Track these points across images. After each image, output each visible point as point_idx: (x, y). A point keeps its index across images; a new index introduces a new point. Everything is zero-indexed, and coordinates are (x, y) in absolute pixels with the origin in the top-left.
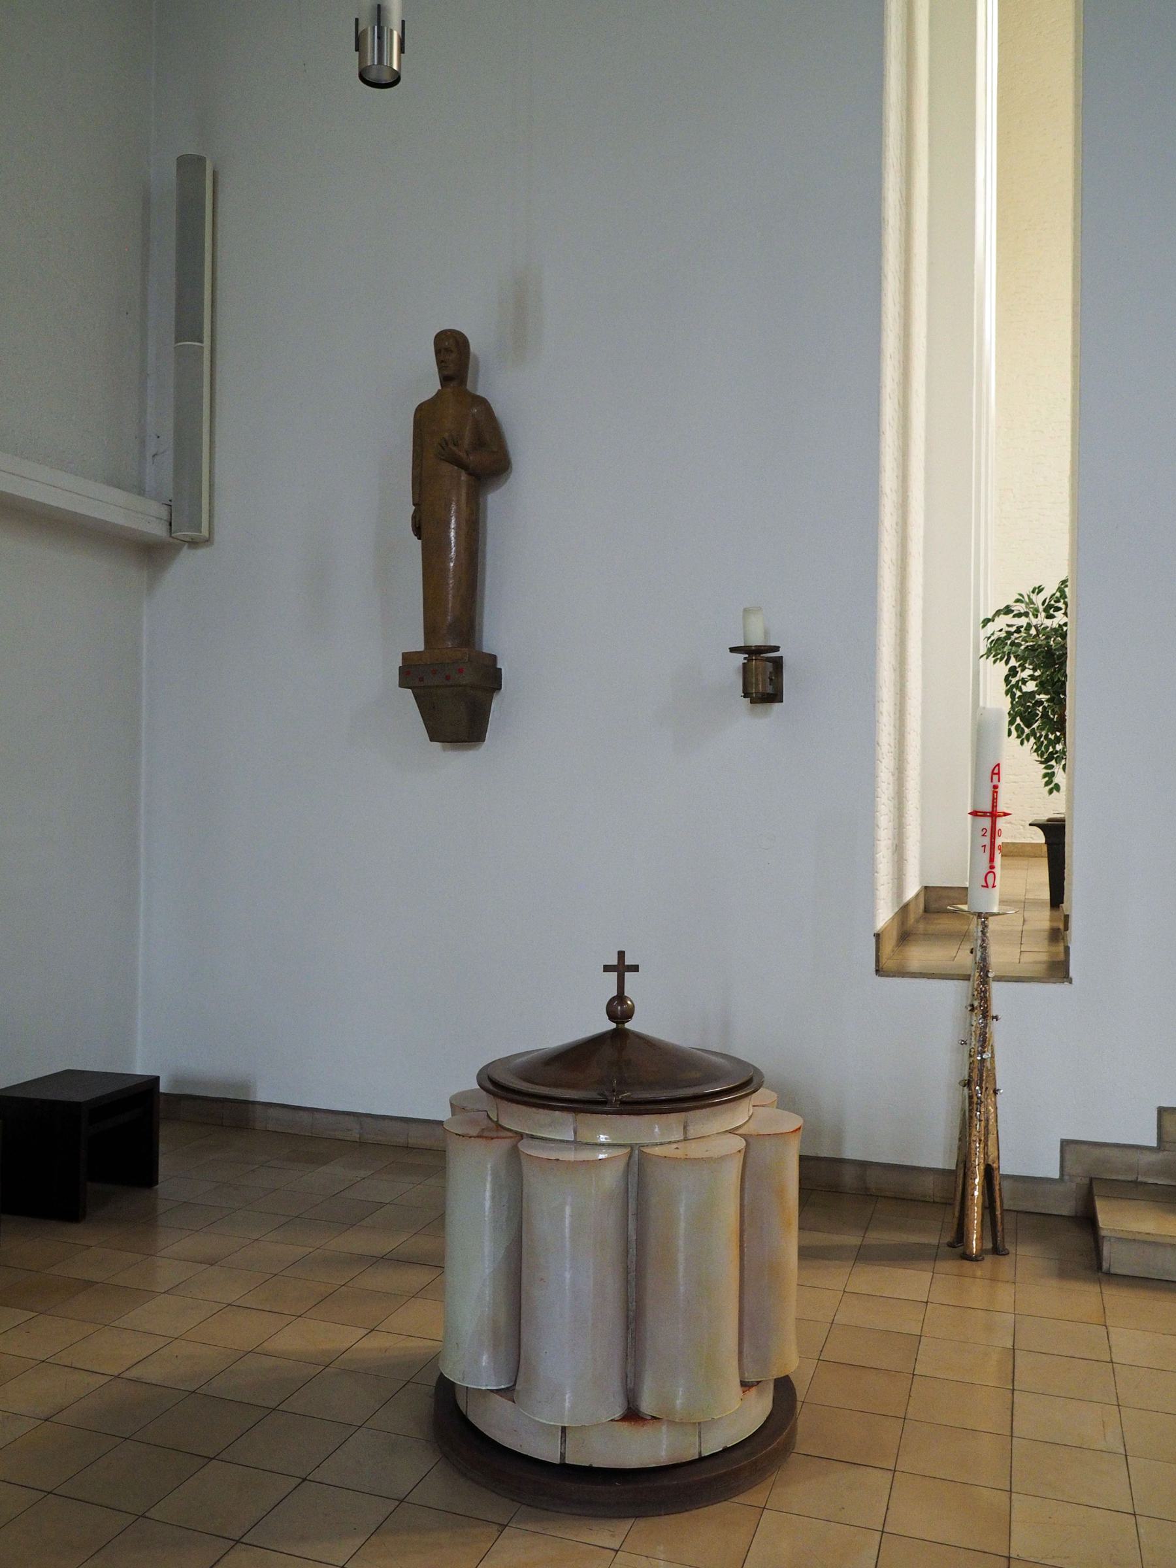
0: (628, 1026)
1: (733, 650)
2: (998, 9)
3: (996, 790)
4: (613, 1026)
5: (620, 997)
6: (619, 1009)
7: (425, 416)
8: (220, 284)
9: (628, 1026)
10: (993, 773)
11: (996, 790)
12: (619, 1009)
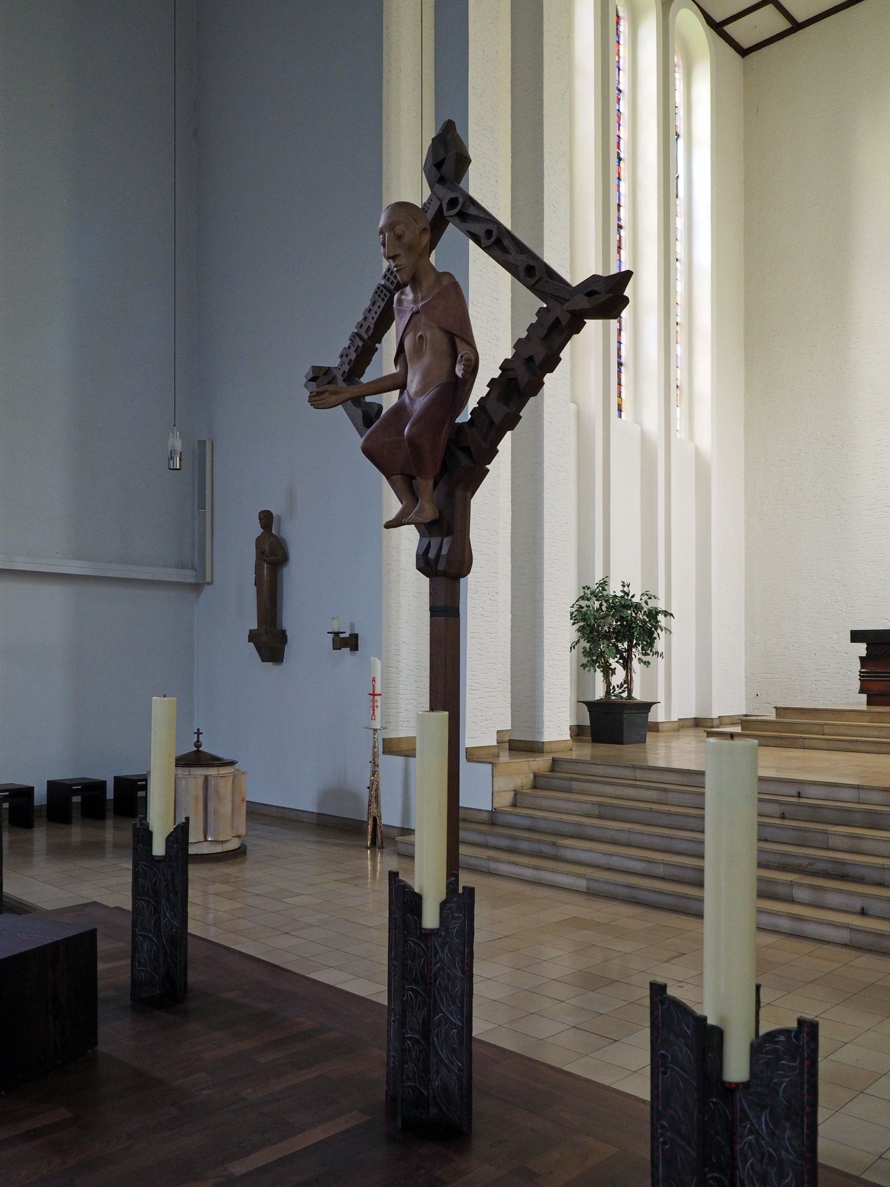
0: (200, 749)
1: (660, 703)
2: (595, 87)
3: (40, 796)
4: (196, 749)
5: (198, 741)
6: (198, 744)
7: (259, 541)
8: (216, 500)
9: (200, 749)
10: (373, 681)
11: (40, 796)
12: (198, 744)
